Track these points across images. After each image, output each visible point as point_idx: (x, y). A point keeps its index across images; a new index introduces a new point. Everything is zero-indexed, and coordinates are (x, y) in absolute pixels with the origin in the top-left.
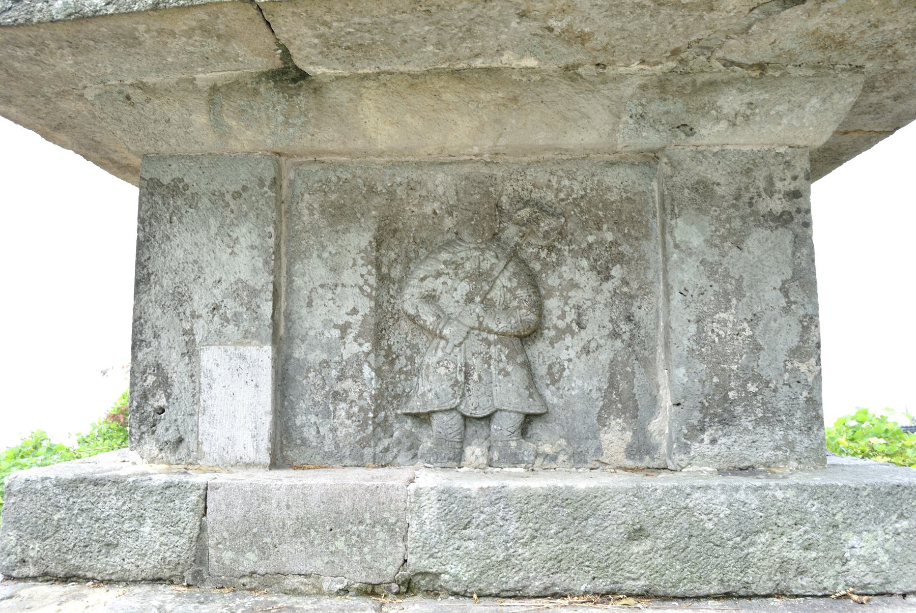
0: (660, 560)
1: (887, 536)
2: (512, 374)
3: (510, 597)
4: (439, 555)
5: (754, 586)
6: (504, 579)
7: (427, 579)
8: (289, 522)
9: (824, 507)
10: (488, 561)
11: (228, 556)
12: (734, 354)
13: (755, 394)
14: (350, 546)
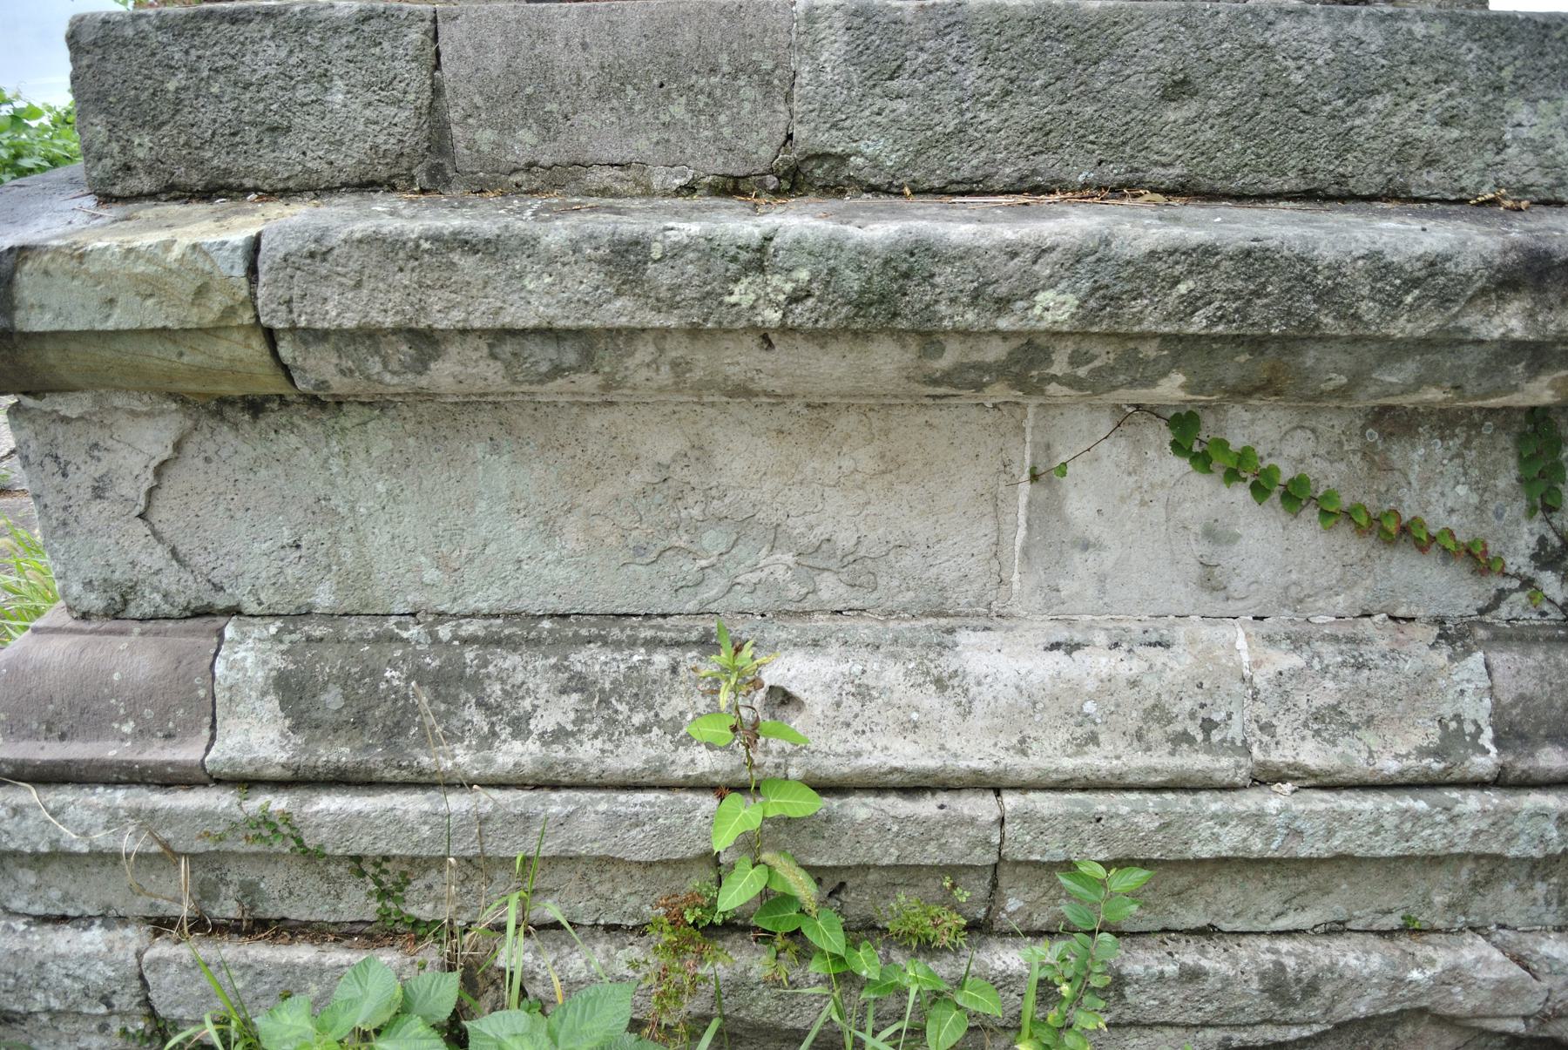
0: (1210, 134)
3: (962, 194)
4: (848, 123)
5: (1352, 182)
6: (954, 164)
7: (826, 166)
8: (588, 74)
9: (1487, 54)
10: (929, 133)
11: (486, 137)
14: (696, 113)
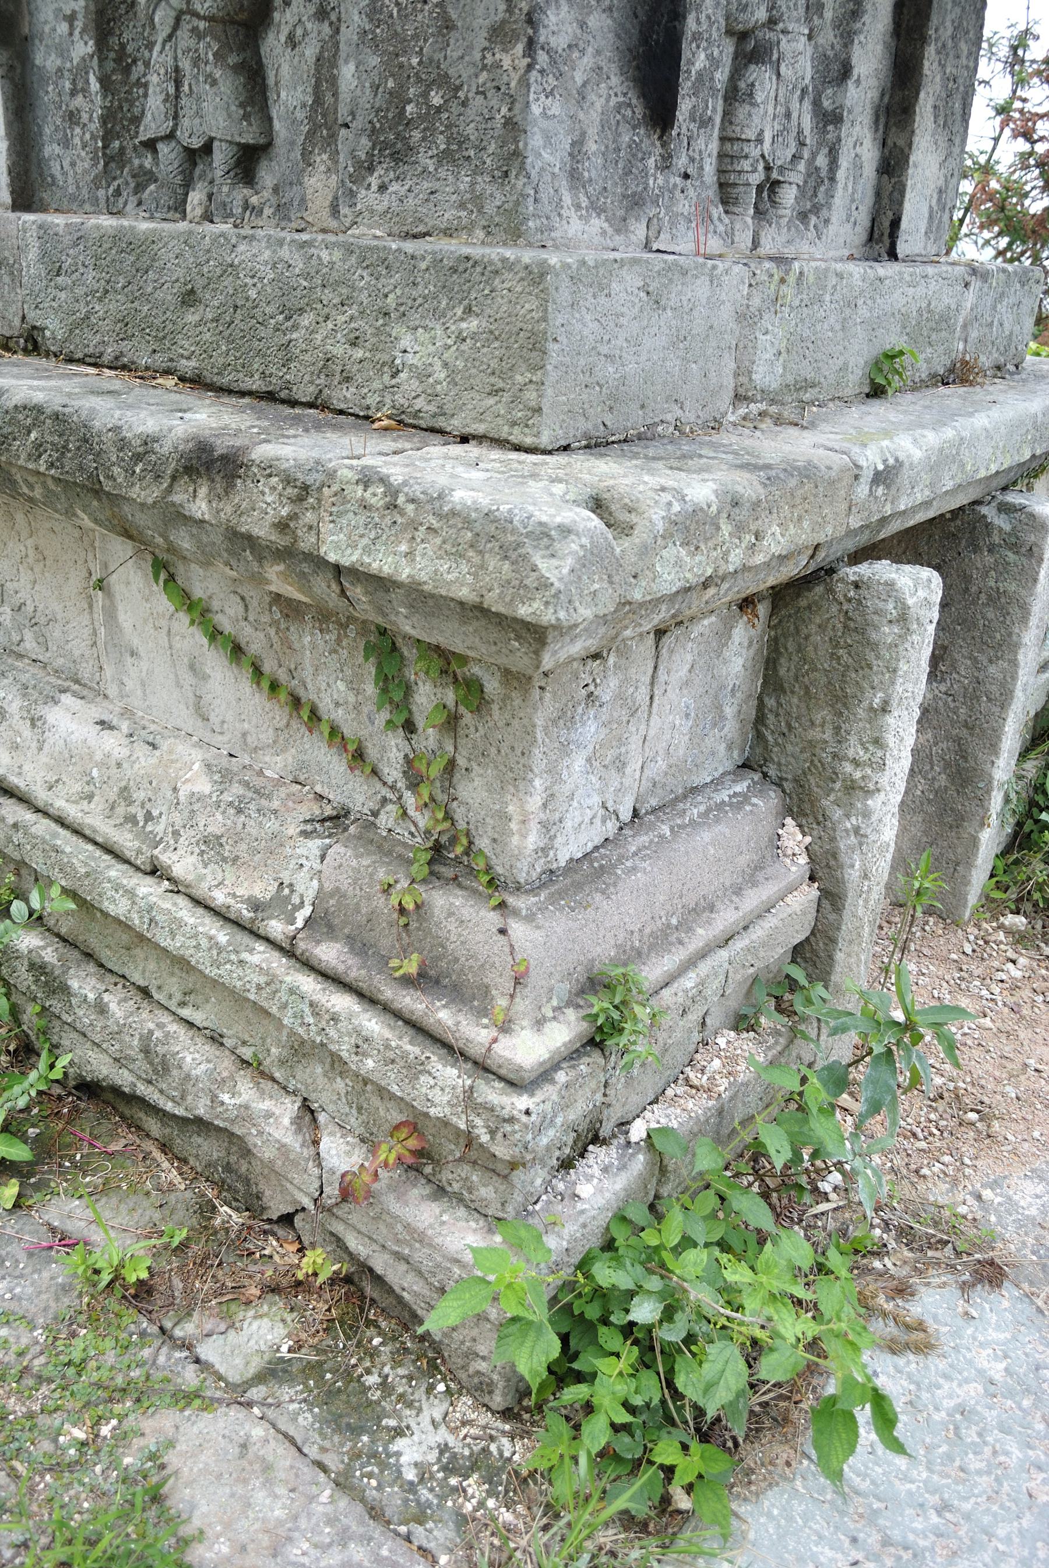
1: (450, 342)
2: (221, 82)
12: (415, 37)
13: (439, 110)
